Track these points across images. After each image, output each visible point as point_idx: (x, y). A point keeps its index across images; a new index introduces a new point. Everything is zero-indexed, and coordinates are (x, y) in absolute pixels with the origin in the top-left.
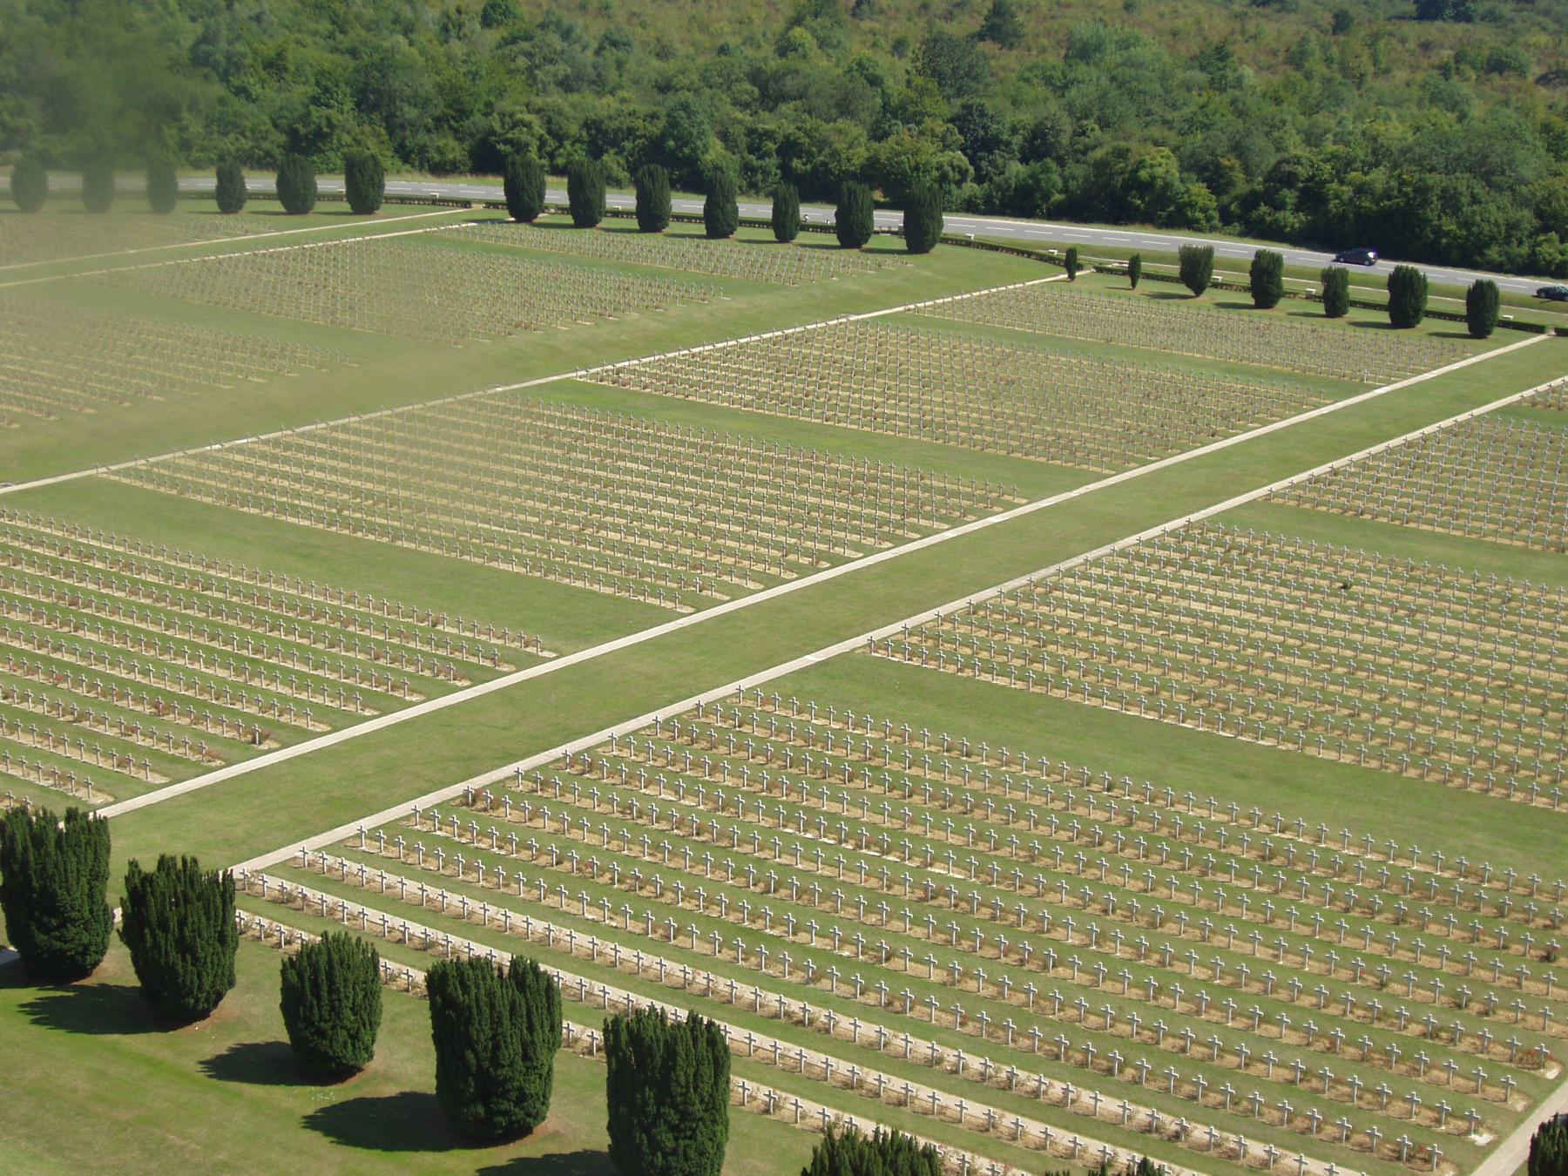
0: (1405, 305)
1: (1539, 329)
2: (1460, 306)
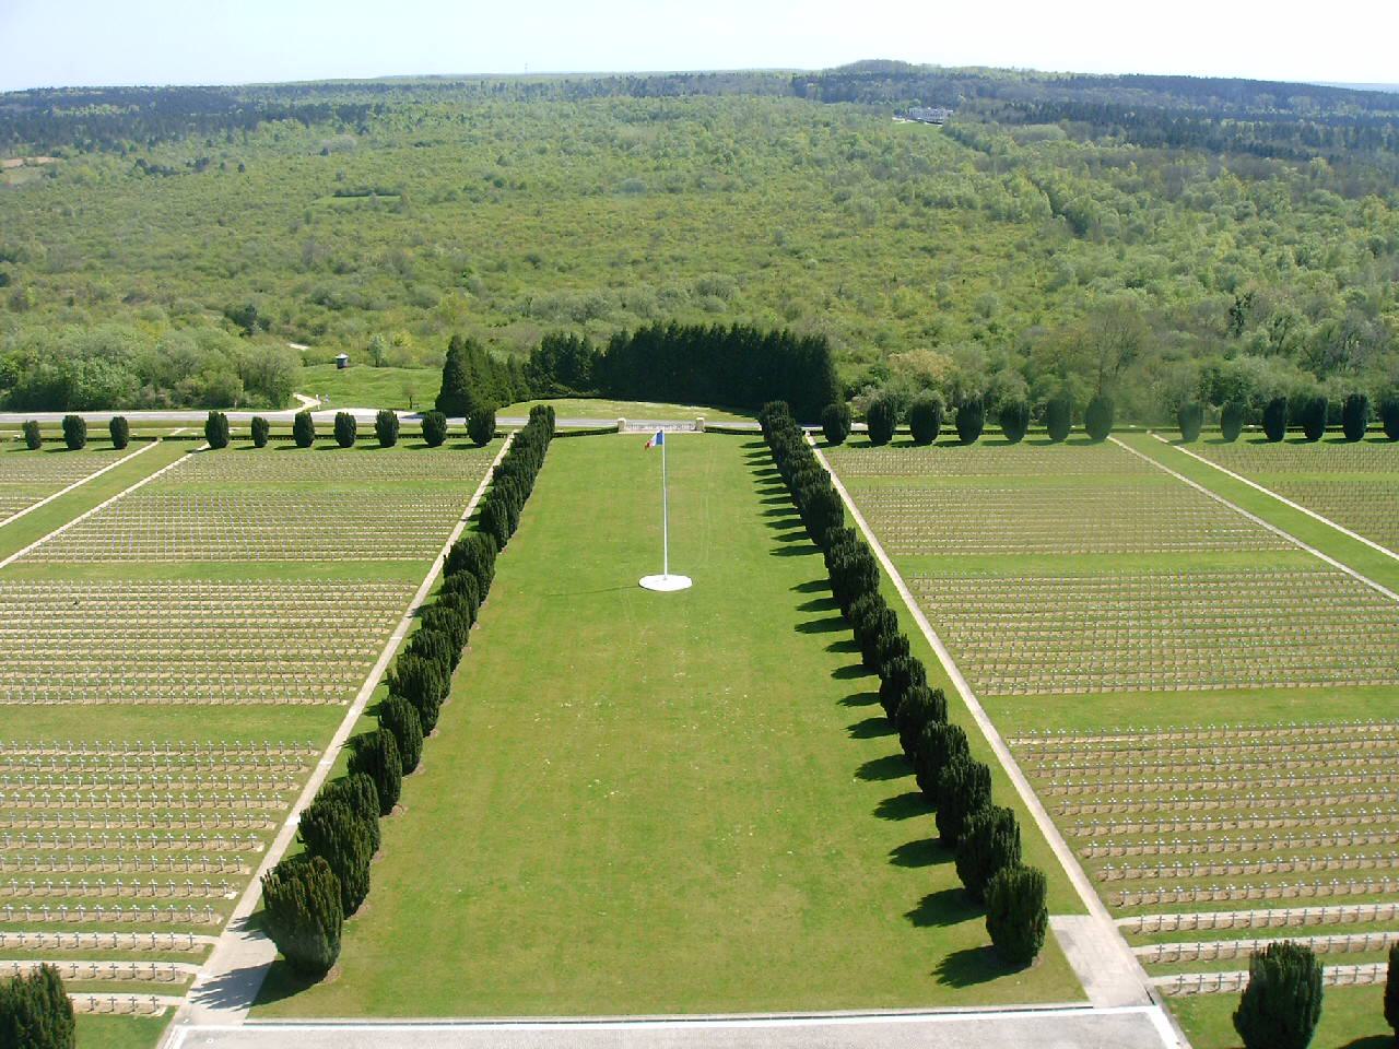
0: (74, 436)
1: (154, 439)
2: (107, 433)
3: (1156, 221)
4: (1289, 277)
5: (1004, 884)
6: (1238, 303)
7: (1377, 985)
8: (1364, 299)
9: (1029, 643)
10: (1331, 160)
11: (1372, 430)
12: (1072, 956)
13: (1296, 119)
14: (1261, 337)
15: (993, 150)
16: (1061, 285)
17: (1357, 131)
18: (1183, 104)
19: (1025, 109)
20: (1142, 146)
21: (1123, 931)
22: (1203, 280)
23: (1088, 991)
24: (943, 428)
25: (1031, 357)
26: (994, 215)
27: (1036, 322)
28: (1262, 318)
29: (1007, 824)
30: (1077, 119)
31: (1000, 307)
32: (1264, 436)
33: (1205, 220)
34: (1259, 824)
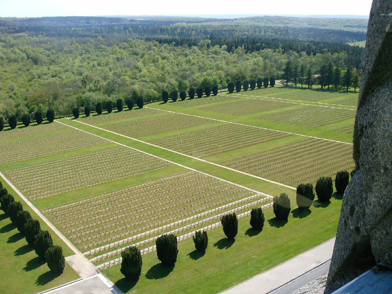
3: (58, 58)
4: (96, 70)
5: (50, 252)
6: (84, 78)
7: (154, 251)
8: (117, 73)
9: (42, 183)
10: (103, 37)
11: (125, 108)
12: (74, 267)
13: (92, 26)
14: (91, 87)
15: (7, 41)
16: (33, 79)
17: (109, 29)
18: (60, 25)
19: (14, 29)
20: (50, 37)
21: (86, 256)
22: (73, 73)
23: (80, 275)
24: (5, 125)
25: (28, 101)
26: (10, 61)
27: (28, 90)
28: (91, 82)
29: (47, 235)
30: (30, 31)
31: (16, 88)
32: (97, 113)
33: (71, 56)
34: (116, 218)
